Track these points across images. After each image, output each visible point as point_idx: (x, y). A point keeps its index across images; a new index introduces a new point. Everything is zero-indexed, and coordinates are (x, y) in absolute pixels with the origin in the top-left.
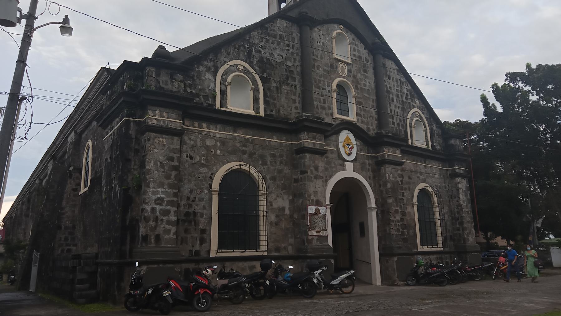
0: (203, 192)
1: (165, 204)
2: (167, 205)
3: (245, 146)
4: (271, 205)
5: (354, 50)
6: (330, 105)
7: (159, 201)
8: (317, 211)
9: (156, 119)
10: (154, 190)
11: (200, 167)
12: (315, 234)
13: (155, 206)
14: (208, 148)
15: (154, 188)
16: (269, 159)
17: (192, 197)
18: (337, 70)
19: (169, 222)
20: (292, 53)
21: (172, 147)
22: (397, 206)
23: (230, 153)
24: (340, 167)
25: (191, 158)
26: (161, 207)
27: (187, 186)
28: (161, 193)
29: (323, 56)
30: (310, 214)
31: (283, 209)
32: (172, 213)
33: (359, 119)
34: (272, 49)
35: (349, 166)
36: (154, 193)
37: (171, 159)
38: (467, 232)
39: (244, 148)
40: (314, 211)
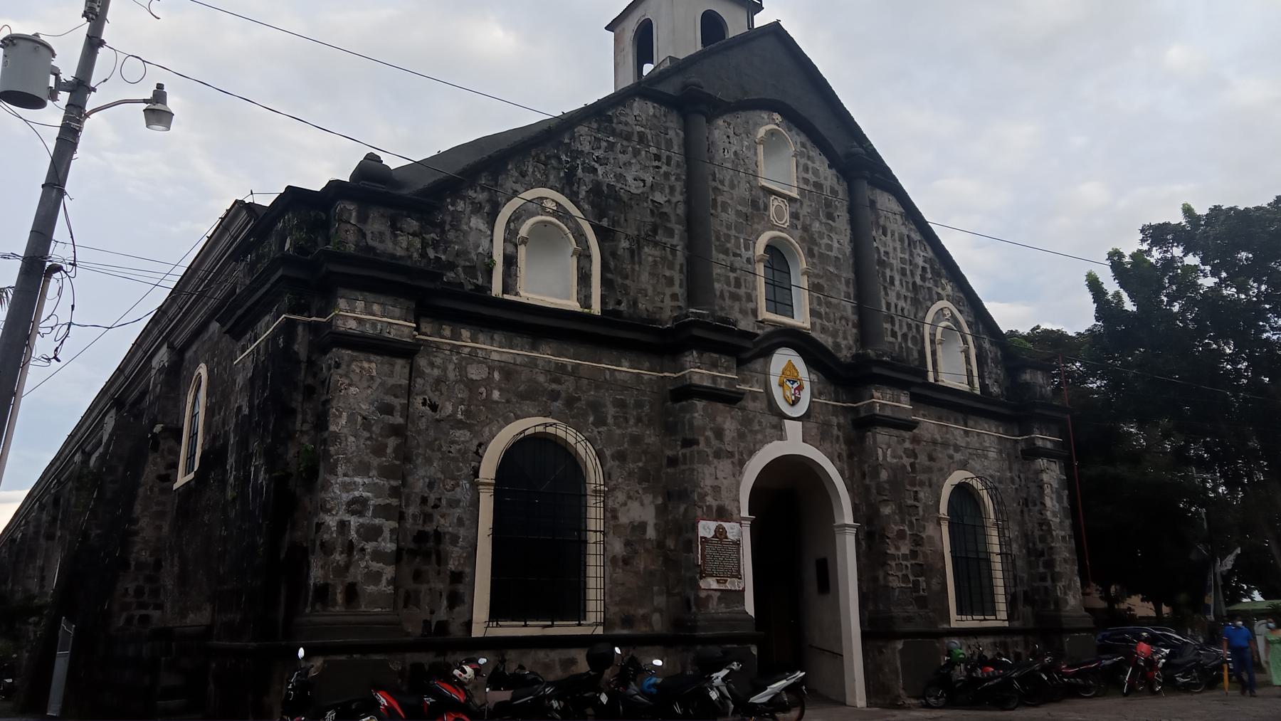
0: (458, 485)
2: (375, 516)
3: (556, 381)
5: (806, 169)
6: (749, 291)
7: (358, 506)
8: (720, 533)
9: (355, 319)
12: (715, 586)
13: (347, 517)
14: (472, 385)
15: (345, 475)
16: (611, 411)
17: (432, 498)
19: (378, 555)
21: (391, 382)
23: (524, 397)
24: (772, 431)
25: (434, 407)
27: (421, 472)
28: (362, 486)
29: (736, 183)
31: (642, 526)
32: (387, 534)
34: (621, 164)
35: (794, 430)
36: (346, 487)
37: (387, 409)
38: (1063, 583)
39: (554, 386)
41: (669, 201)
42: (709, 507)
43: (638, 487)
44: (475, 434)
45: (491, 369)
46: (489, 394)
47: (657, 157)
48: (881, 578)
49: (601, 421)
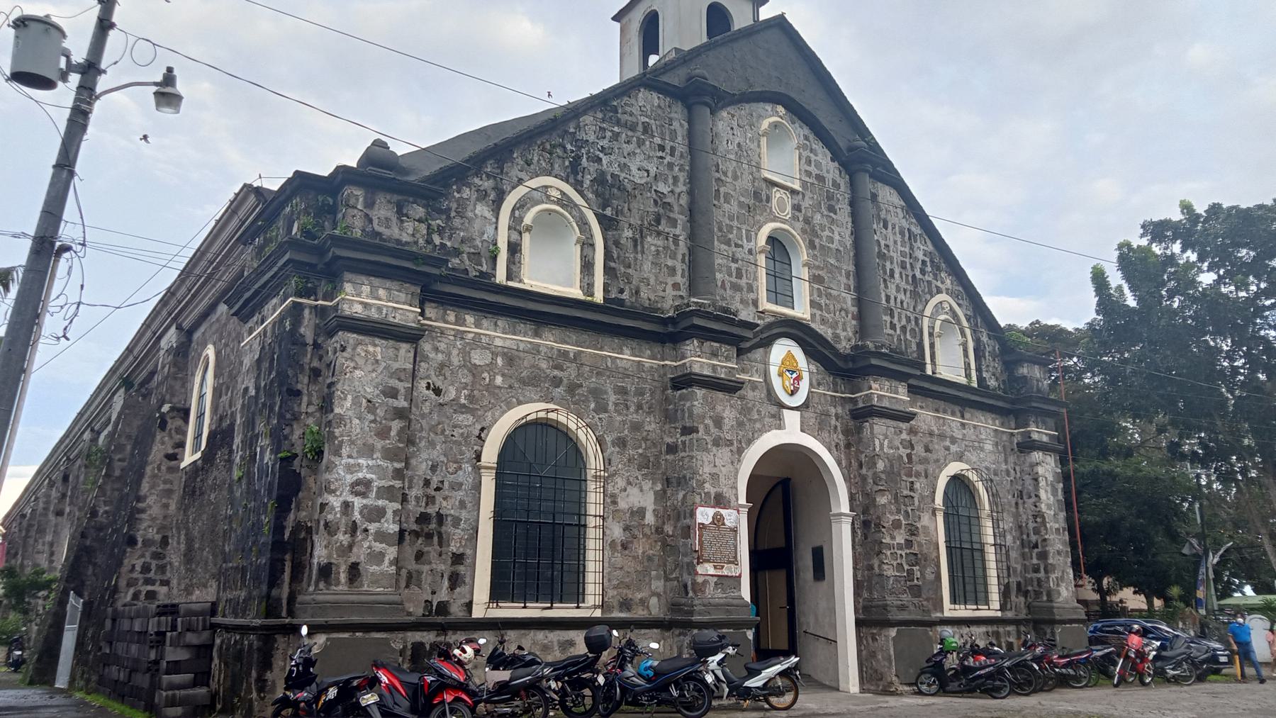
0: (460, 468)
3: (558, 367)
5: (809, 162)
7: (361, 487)
8: (718, 520)
10: (351, 461)
11: (455, 412)
12: (712, 571)
13: (350, 498)
14: (474, 370)
15: (350, 457)
18: (769, 205)
19: (381, 536)
20: (670, 166)
21: (396, 365)
23: (524, 382)
25: (438, 392)
26: (365, 501)
28: (366, 468)
30: (702, 526)
31: (641, 512)
32: (389, 514)
34: (626, 155)
35: (792, 419)
36: (350, 469)
37: (392, 393)
41: (672, 191)
43: (637, 473)
44: (478, 419)
45: (495, 355)
46: (492, 380)
49: (602, 408)
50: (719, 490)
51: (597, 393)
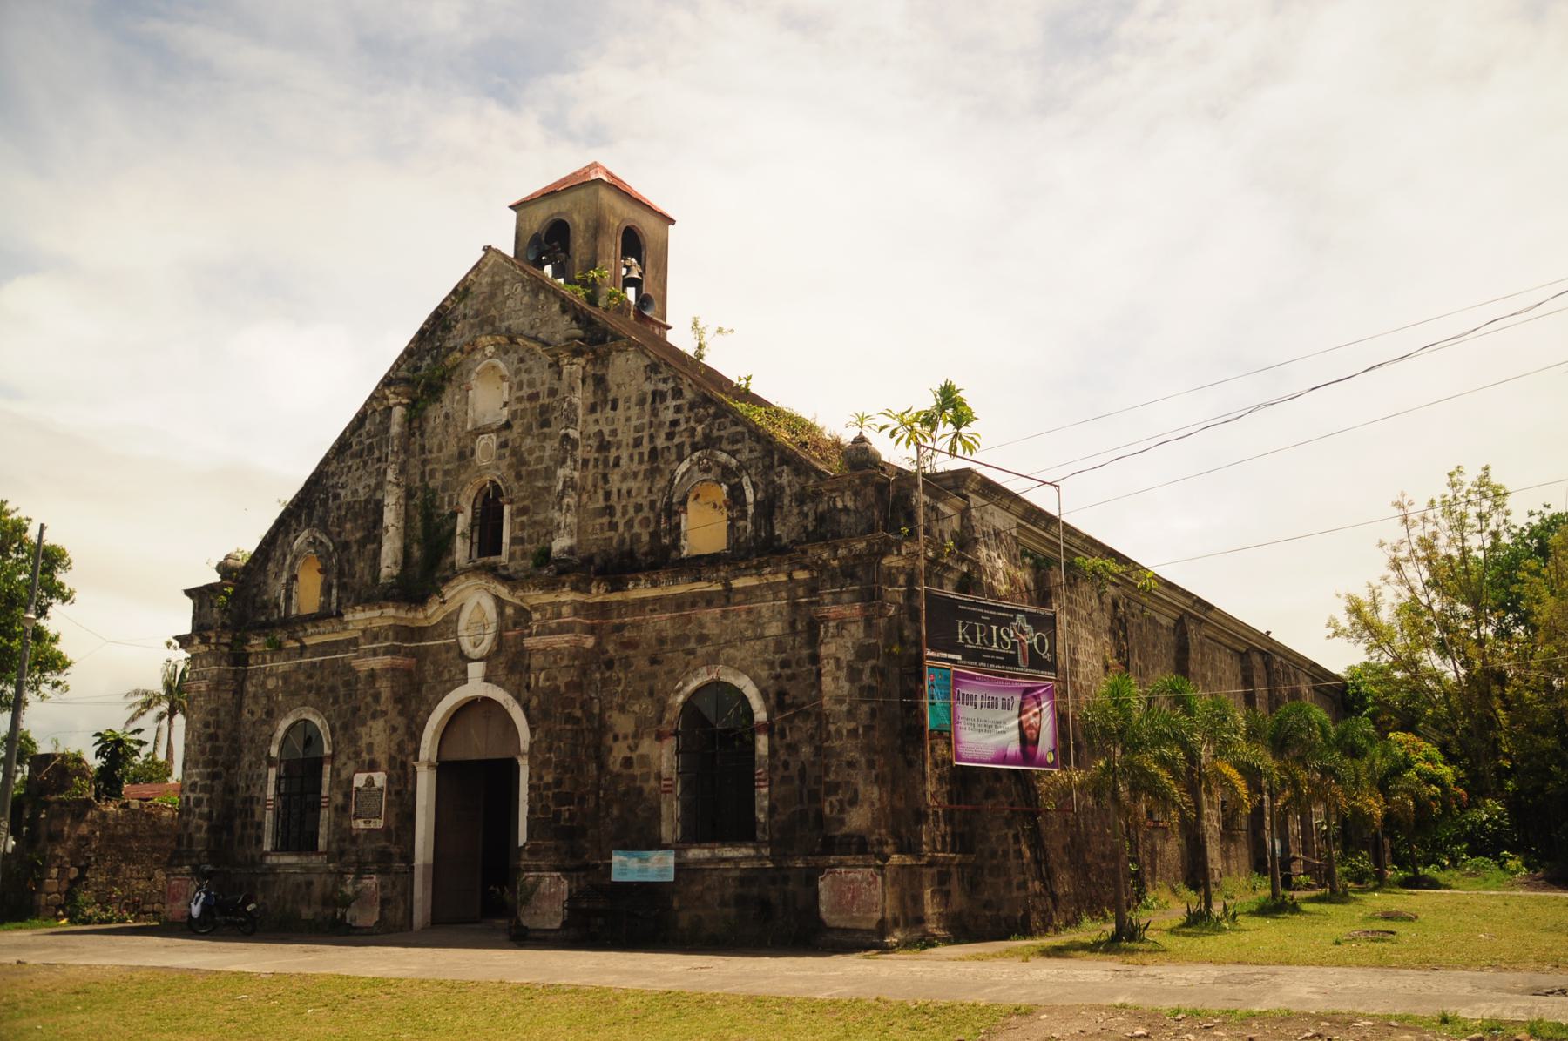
1: (198, 791)
2: (201, 791)
4: (339, 775)
8: (370, 782)
9: (829, 594)
12: (362, 825)
22: (550, 750)
27: (246, 759)
29: (444, 444)
30: (358, 789)
33: (515, 552)
35: (476, 670)
38: (840, 796)
40: (364, 783)
42: (364, 761)
47: (379, 460)
48: (258, 813)
49: (336, 701)
50: (372, 756)
51: (333, 689)
